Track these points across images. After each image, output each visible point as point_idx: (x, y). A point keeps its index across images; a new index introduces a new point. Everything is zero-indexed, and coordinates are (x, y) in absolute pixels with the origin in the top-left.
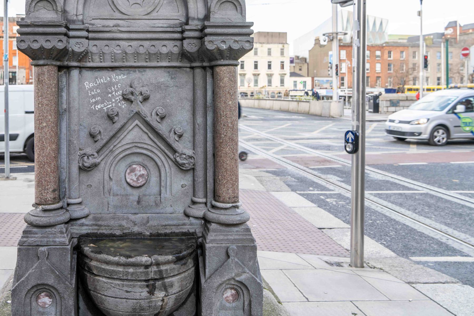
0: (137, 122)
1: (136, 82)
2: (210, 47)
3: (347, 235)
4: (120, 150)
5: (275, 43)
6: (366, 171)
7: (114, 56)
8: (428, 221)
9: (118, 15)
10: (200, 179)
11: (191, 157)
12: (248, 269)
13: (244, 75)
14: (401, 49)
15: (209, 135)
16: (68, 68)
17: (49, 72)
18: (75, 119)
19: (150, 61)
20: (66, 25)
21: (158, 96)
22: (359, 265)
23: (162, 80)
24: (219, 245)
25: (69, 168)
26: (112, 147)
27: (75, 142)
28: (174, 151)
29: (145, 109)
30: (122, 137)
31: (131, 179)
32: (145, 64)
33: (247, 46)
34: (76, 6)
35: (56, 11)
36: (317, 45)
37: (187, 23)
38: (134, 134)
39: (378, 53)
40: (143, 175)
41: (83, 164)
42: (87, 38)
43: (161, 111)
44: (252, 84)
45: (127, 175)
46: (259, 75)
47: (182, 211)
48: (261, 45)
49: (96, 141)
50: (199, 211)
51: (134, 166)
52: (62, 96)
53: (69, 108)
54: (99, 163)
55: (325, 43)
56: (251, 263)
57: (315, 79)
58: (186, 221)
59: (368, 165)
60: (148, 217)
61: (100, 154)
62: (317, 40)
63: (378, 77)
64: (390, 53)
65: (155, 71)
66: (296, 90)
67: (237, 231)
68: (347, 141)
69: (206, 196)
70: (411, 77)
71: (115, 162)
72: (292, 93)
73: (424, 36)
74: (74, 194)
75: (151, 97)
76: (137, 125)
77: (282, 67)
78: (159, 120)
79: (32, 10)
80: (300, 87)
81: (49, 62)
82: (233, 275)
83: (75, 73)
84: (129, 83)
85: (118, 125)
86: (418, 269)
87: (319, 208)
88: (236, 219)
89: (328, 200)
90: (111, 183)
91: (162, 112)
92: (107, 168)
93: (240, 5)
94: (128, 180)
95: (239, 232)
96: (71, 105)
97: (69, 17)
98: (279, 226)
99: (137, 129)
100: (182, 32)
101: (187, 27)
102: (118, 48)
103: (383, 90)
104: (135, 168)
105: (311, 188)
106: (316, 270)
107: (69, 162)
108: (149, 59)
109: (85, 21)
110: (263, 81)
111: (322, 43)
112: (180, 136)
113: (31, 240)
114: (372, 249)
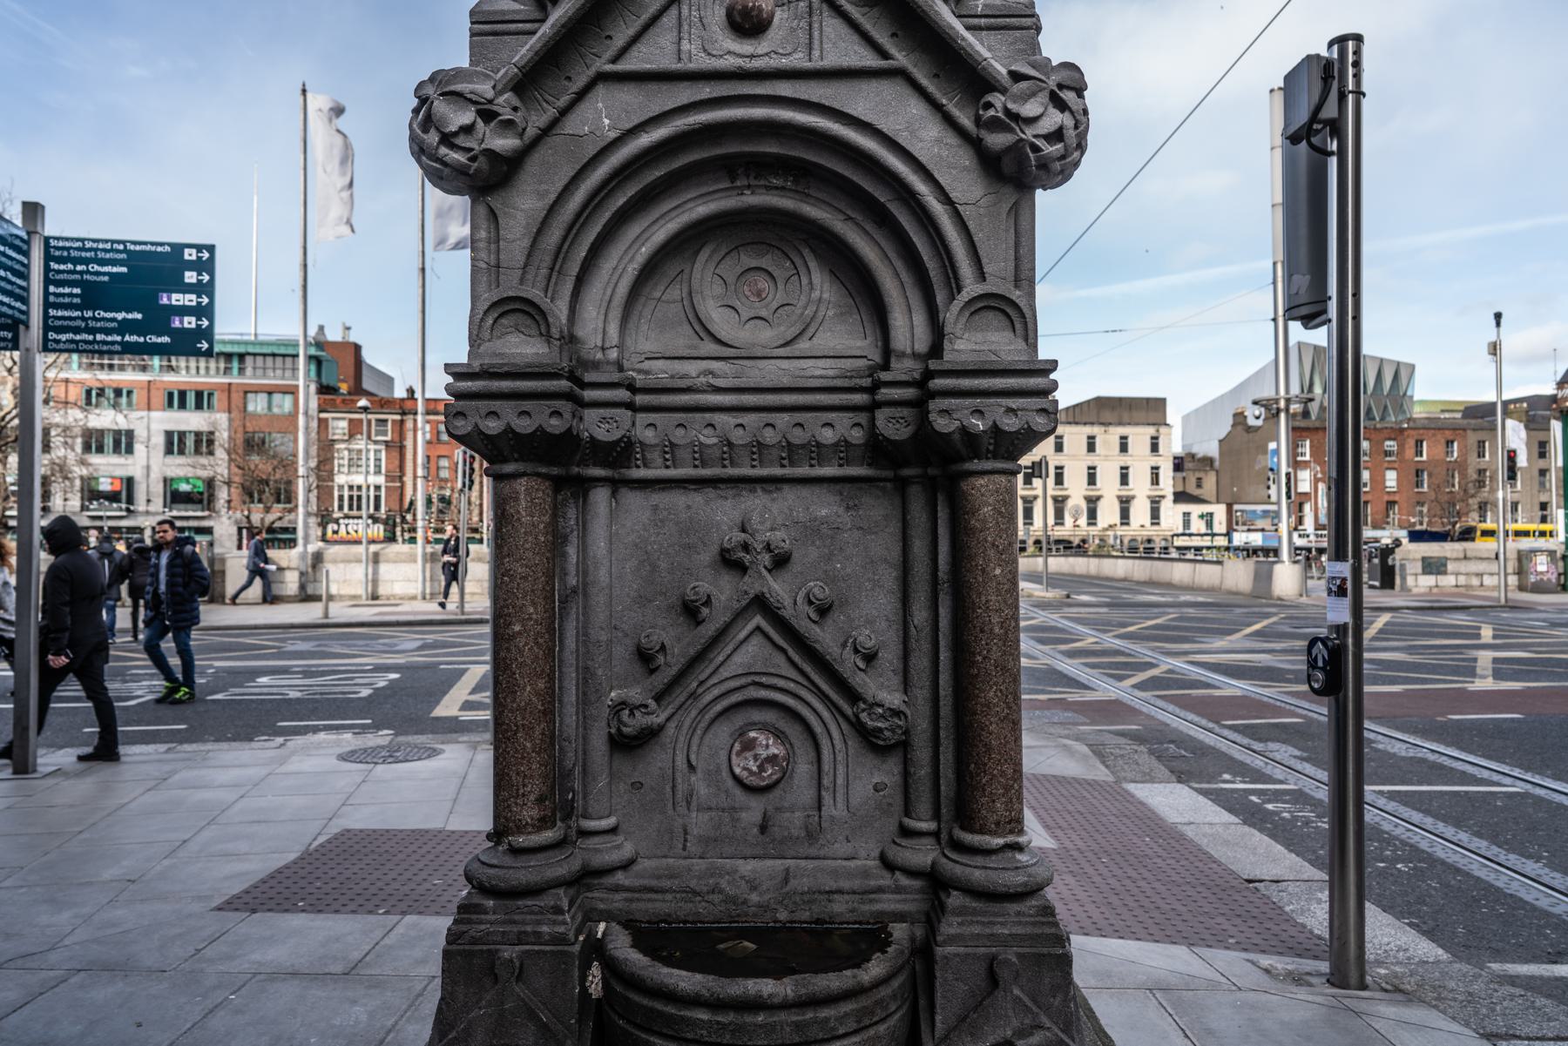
0: (758, 620)
1: (755, 518)
2: (942, 424)
3: (1319, 901)
4: (716, 692)
5: (1137, 424)
6: (1366, 734)
7: (701, 453)
8: (1531, 867)
9: (710, 348)
10: (923, 772)
11: (897, 713)
12: (1050, 1018)
13: (1066, 498)
14: (1448, 434)
15: (944, 655)
16: (581, 488)
17: (529, 493)
18: (600, 616)
19: (792, 464)
20: (571, 372)
21: (813, 553)
22: (1353, 980)
23: (824, 512)
24: (969, 950)
25: (585, 738)
26: (695, 684)
27: (600, 672)
28: (854, 696)
29: (778, 588)
30: (721, 658)
31: (745, 769)
32: (778, 471)
33: (1040, 422)
34: (601, 325)
35: (547, 337)
36: (1239, 428)
37: (886, 366)
38: (750, 653)
39: (1390, 445)
40: (775, 756)
41: (619, 729)
42: (630, 406)
43: (820, 591)
44: (1083, 521)
45: (734, 757)
46: (1098, 498)
47: (876, 853)
48: (1103, 428)
49: (652, 672)
50: (922, 855)
51: (752, 734)
52: (564, 555)
53: (585, 585)
54: (661, 728)
55: (1259, 423)
56: (1057, 1002)
57: (1236, 507)
58: (886, 880)
59: (1370, 718)
60: (787, 870)
61: (664, 703)
62: (1239, 418)
63: (1391, 504)
64: (1419, 443)
65: (805, 491)
66: (1190, 535)
67: (1018, 914)
68: (1312, 664)
69: (936, 816)
70: (1474, 502)
71: (703, 725)
72: (1179, 542)
73: (1506, 404)
74: (594, 807)
75: (796, 556)
76: (758, 628)
77: (1155, 480)
78: (814, 616)
79: (486, 335)
80: (1198, 526)
81: (529, 468)
82: (1009, 1033)
83: (600, 496)
84: (738, 521)
85: (708, 630)
86: (1512, 997)
87: (1247, 829)
88: (1017, 880)
89: (1270, 807)
90: (693, 779)
91: (821, 596)
92: (682, 739)
93: (1023, 316)
94: (737, 771)
95: (1024, 915)
96: (591, 578)
97: (584, 354)
98: (1147, 874)
99: (757, 640)
100: (873, 389)
101: (885, 376)
102: (709, 431)
103: (1402, 534)
104: (755, 739)
105: (1226, 776)
106: (1239, 994)
107: (585, 722)
108: (790, 458)
109: (626, 364)
110: (1108, 513)
111: (1251, 422)
112: (870, 658)
113: (476, 930)
114: (1386, 940)
